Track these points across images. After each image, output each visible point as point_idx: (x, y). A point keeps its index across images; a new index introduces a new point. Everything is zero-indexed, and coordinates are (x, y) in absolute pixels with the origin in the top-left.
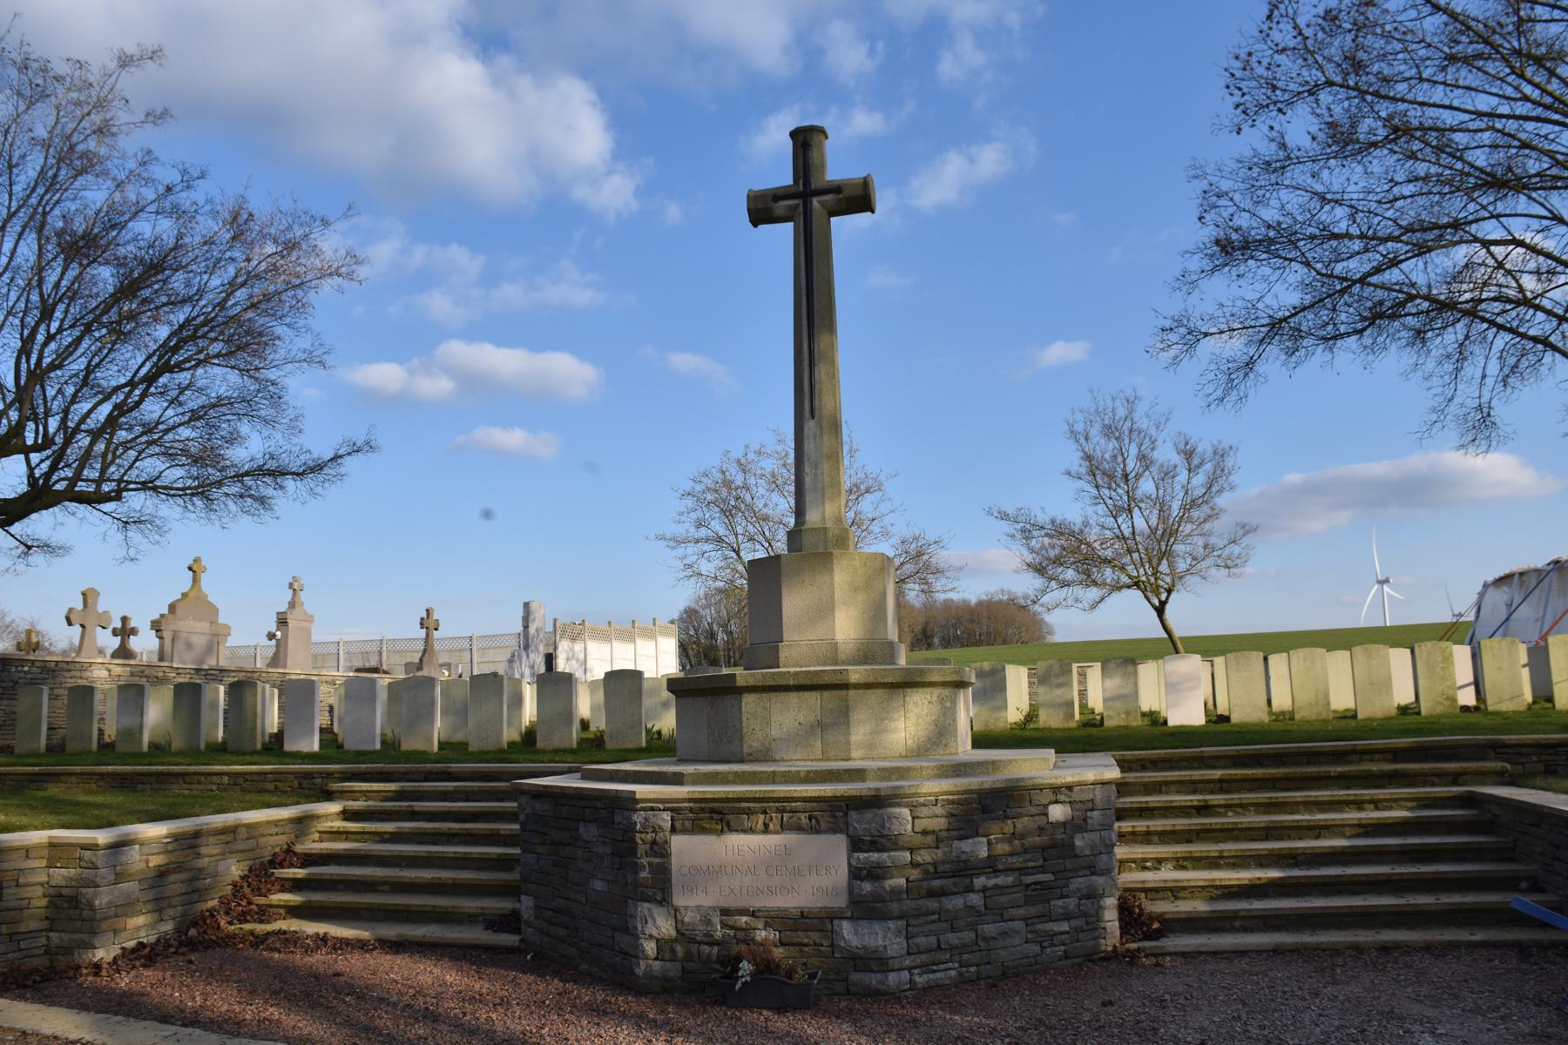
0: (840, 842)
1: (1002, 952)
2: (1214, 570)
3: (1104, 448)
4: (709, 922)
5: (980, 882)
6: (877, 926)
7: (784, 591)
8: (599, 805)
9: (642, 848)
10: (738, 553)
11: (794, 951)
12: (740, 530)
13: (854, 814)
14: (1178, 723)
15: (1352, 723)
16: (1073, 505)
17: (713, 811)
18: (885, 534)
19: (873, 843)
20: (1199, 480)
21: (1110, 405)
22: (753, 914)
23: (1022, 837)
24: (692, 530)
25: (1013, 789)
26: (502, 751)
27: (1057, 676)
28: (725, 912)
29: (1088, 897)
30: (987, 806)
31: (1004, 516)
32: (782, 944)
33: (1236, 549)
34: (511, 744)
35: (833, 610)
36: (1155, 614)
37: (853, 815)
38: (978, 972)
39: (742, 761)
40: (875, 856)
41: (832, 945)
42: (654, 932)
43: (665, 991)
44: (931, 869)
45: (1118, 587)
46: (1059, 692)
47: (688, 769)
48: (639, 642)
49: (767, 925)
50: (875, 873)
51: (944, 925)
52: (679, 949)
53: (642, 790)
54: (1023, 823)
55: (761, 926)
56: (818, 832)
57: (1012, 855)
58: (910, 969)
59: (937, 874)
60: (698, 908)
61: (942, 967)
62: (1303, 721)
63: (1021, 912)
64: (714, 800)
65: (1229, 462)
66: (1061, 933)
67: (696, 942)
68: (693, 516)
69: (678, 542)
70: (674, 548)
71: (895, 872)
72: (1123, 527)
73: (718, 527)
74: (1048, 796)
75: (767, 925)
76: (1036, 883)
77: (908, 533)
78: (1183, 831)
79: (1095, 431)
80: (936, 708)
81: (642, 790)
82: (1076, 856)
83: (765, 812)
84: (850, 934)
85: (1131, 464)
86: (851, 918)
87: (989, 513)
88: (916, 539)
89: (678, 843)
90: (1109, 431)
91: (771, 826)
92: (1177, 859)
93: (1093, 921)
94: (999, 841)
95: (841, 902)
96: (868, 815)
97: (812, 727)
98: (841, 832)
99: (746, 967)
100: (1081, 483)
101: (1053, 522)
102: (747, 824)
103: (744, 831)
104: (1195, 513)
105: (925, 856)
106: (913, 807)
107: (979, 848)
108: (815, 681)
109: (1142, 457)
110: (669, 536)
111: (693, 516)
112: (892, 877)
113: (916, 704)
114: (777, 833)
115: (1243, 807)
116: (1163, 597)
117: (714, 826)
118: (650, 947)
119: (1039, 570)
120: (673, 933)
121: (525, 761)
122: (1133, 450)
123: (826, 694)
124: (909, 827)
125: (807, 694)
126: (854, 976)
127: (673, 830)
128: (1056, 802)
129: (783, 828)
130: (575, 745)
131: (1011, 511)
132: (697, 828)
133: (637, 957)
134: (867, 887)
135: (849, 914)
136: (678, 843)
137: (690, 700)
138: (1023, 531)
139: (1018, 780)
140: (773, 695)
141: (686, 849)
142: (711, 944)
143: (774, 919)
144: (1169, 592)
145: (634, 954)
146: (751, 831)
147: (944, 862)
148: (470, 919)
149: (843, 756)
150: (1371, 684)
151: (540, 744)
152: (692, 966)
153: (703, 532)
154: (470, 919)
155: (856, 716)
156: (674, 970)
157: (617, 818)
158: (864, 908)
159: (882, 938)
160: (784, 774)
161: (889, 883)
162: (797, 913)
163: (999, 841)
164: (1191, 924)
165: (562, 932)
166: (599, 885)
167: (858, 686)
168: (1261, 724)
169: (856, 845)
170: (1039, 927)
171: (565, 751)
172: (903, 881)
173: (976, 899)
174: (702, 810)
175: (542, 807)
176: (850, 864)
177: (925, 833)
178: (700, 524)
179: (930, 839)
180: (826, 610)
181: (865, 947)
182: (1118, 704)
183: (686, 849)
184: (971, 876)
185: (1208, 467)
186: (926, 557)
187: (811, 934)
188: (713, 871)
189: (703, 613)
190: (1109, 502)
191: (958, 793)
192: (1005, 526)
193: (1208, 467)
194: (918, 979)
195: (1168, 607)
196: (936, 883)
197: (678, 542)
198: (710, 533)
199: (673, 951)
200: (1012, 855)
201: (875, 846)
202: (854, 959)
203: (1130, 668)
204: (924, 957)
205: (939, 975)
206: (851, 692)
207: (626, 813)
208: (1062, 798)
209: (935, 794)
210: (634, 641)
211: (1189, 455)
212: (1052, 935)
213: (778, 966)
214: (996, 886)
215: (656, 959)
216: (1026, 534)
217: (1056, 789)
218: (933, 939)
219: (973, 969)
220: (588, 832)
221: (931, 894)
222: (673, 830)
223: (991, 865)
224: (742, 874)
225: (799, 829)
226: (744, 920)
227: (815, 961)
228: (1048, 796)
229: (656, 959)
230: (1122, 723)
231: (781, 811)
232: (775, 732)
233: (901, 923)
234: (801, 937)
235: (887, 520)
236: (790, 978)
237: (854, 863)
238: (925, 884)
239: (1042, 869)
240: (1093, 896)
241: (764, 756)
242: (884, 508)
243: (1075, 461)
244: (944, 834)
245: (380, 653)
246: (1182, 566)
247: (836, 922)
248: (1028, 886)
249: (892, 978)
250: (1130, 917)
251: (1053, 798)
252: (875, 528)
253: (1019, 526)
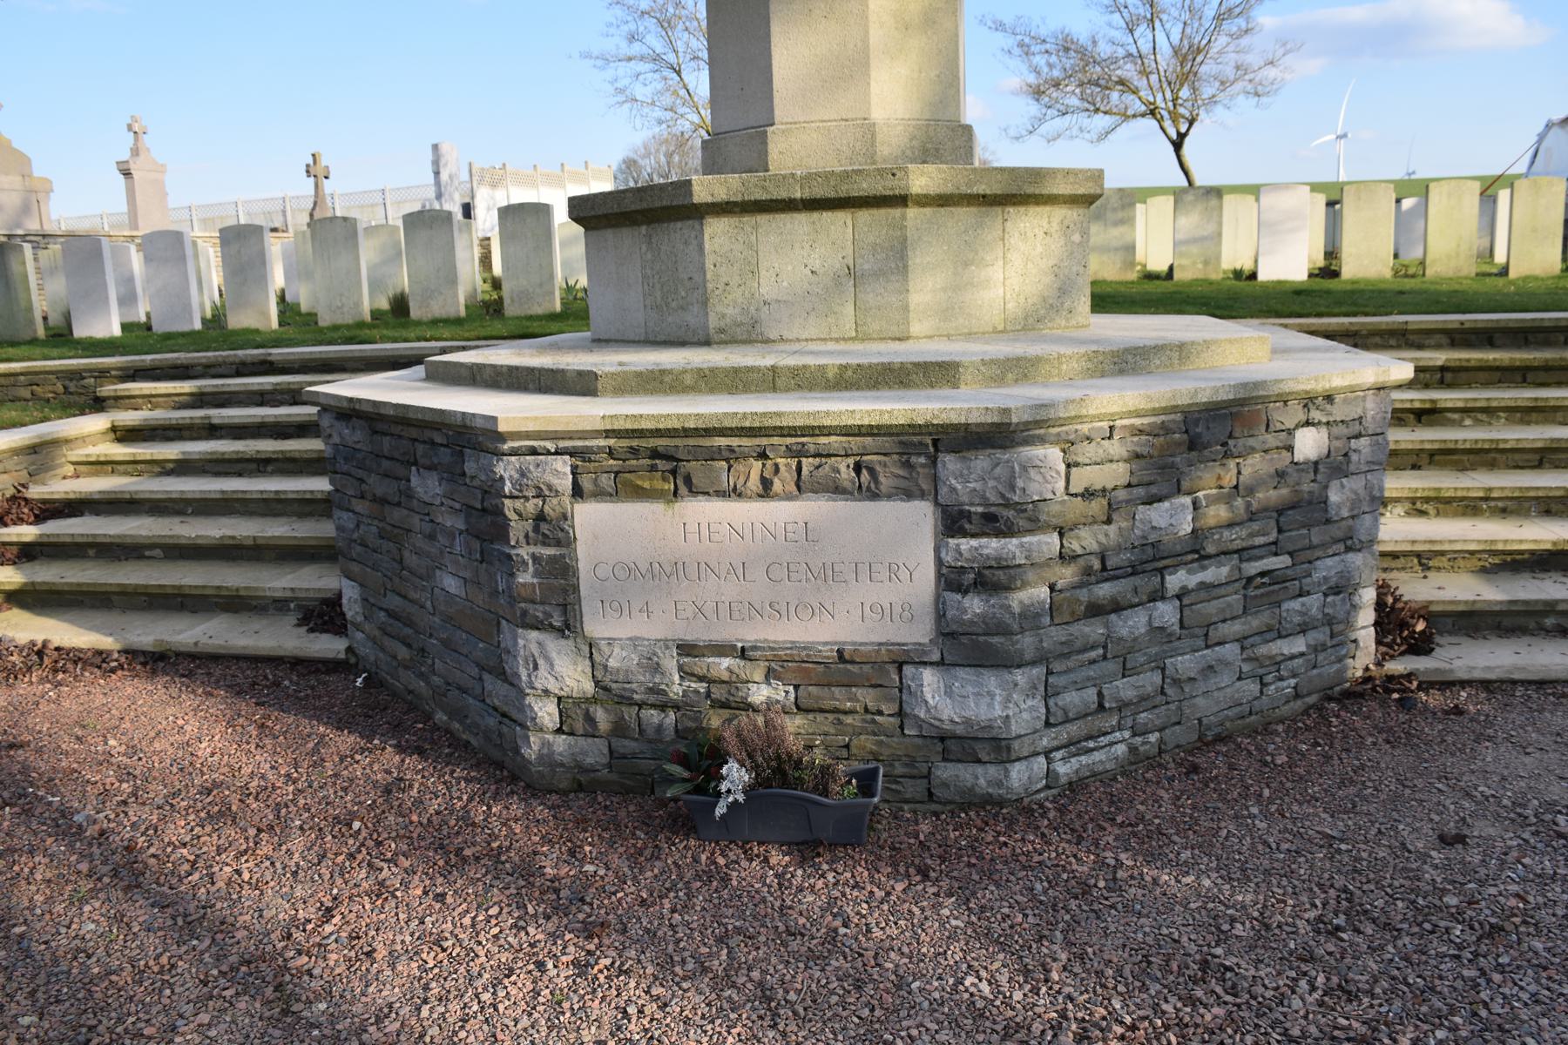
0: (920, 516)
1: (1200, 701)
2: (1241, 98)
4: (656, 668)
5: (1177, 580)
6: (991, 680)
7: (776, 29)
8: (439, 439)
9: (517, 529)
10: (679, 73)
11: (825, 722)
12: (680, 46)
13: (948, 464)
14: (1275, 277)
15: (1501, 281)
17: (655, 454)
19: (990, 518)
22: (743, 654)
23: (1251, 491)
24: (624, 44)
25: (1241, 402)
26: (361, 325)
27: (1114, 210)
28: (687, 649)
29: (1336, 590)
30: (1202, 433)
31: (1000, 26)
32: (799, 708)
33: (1271, 73)
34: (376, 314)
36: (1171, 148)
37: (950, 463)
38: (1161, 741)
39: (706, 343)
40: (992, 546)
41: (901, 713)
42: (553, 686)
43: (580, 787)
44: (1097, 565)
45: (1126, 117)
46: (1115, 232)
47: (604, 362)
49: (770, 675)
50: (990, 579)
51: (1112, 666)
52: (602, 716)
53: (510, 411)
54: (1254, 466)
55: (758, 676)
56: (874, 496)
57: (1230, 525)
58: (1047, 753)
59: (1106, 572)
60: (634, 641)
61: (1104, 740)
62: (1439, 280)
63: (1236, 628)
64: (657, 433)
66: (1293, 657)
67: (631, 703)
68: (625, 28)
69: (605, 60)
70: (602, 68)
71: (1031, 575)
73: (656, 43)
74: (1295, 414)
75: (770, 675)
76: (1262, 574)
78: (1409, 452)
80: (1057, 245)
81: (510, 411)
82: (1328, 521)
83: (763, 456)
84: (939, 696)
86: (940, 663)
89: (589, 518)
91: (777, 486)
92: (1413, 501)
93: (1337, 629)
94: (1212, 501)
95: (919, 633)
96: (981, 462)
97: (837, 281)
98: (922, 495)
99: (735, 776)
102: (724, 482)
103: (722, 494)
105: (1086, 540)
106: (1067, 445)
107: (1173, 518)
108: (844, 190)
110: (596, 53)
111: (625, 28)
112: (1025, 585)
113: (1023, 235)
114: (789, 497)
115: (1489, 412)
116: (1183, 130)
117: (660, 485)
118: (547, 712)
119: (1037, 93)
120: (589, 687)
121: (383, 339)
123: (864, 215)
124: (1061, 484)
125: (827, 216)
126: (946, 772)
127: (578, 492)
128: (1308, 423)
129: (801, 487)
130: (463, 313)
131: (1008, 20)
132: (625, 489)
133: (523, 726)
134: (975, 605)
135: (936, 657)
136: (589, 518)
137: (609, 234)
139: (1257, 385)
140: (763, 219)
141: (604, 529)
142: (662, 707)
143: (780, 664)
144: (1191, 123)
145: (515, 719)
146: (736, 493)
147: (1119, 549)
148: (274, 606)
149: (895, 331)
150: (1535, 230)
151: (415, 313)
152: (628, 746)
153: (637, 48)
154: (274, 606)
155: (917, 259)
156: (594, 753)
157: (470, 467)
158: (966, 647)
159: (999, 701)
160: (795, 372)
161: (1019, 599)
162: (830, 653)
163: (1212, 501)
164: (1474, 622)
165: (403, 653)
166: (451, 584)
167: (926, 201)
168: (1383, 281)
169: (953, 522)
170: (1263, 650)
171: (447, 322)
172: (1043, 592)
173: (1166, 613)
174: (634, 452)
175: (354, 435)
176: (939, 562)
177: (1088, 494)
178: (632, 38)
179: (1097, 507)
180: (851, 68)
181: (967, 722)
182: (1194, 249)
183: (604, 529)
184: (1161, 571)
187: (859, 692)
188: (659, 574)
189: (641, 162)
191: (1155, 412)
194: (1062, 769)
195: (1187, 140)
196: (1105, 591)
197: (605, 60)
198: (645, 51)
199: (590, 719)
200: (1230, 525)
201: (993, 524)
202: (942, 739)
203: (1214, 202)
204: (1074, 729)
205: (1097, 756)
206: (912, 212)
207: (485, 459)
208: (1316, 415)
209: (1112, 417)
212: (1277, 662)
213: (798, 764)
214: (1203, 586)
215: (559, 731)
217: (1309, 401)
218: (1091, 694)
219: (1153, 737)
220: (427, 486)
221: (1096, 610)
222: (578, 492)
223: (1196, 550)
224: (727, 585)
225: (837, 490)
226: (723, 665)
227: (866, 742)
228: (1295, 414)
229: (559, 731)
230: (1201, 276)
231: (798, 453)
232: (767, 289)
233: (1038, 671)
234: (838, 697)
236: (825, 793)
237: (948, 558)
238: (1083, 595)
239: (1275, 549)
240: (1343, 588)
241: (749, 334)
244: (1122, 495)
245: (284, 212)
246: (1207, 91)
247: (908, 670)
248: (1250, 579)
249: (1018, 776)
250: (1394, 623)
251: (1302, 417)
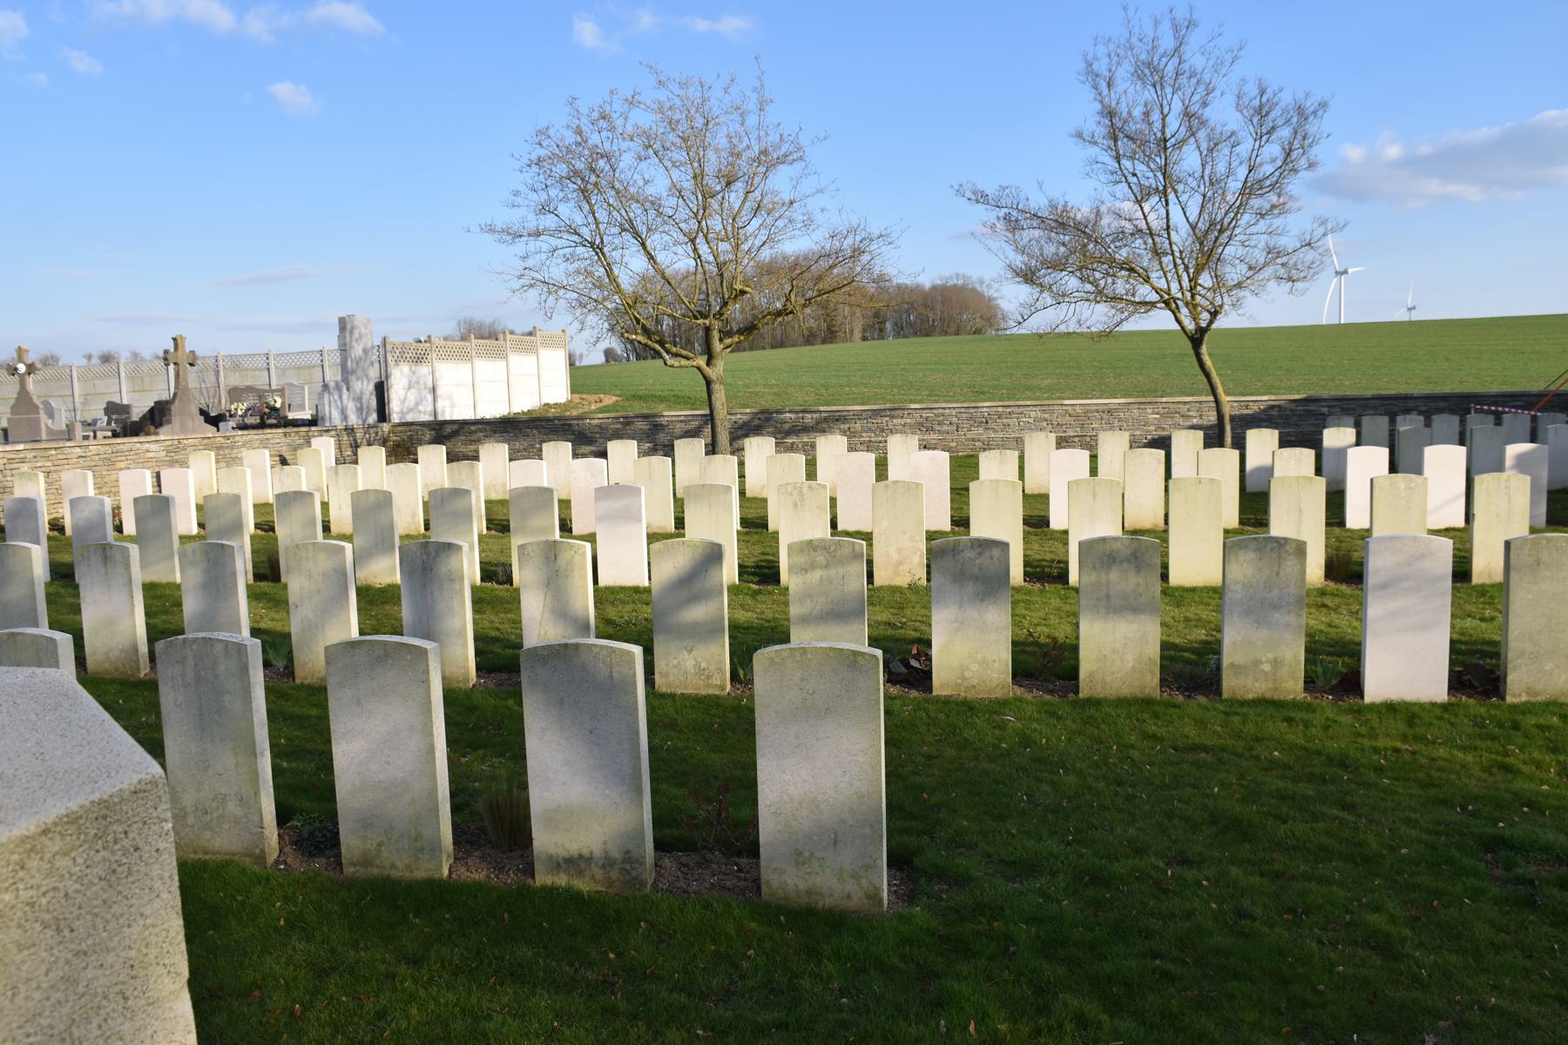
2: (1272, 283)
3: (1132, 97)
16: (1085, 186)
18: (808, 224)
20: (1273, 150)
21: (1151, 33)
24: (531, 216)
31: (981, 198)
35: (354, 514)
36: (1189, 345)
48: (543, 352)
65: (1312, 127)
72: (1151, 217)
77: (841, 224)
79: (1123, 73)
85: (1173, 123)
87: (960, 192)
88: (853, 231)
90: (1150, 72)
100: (1095, 151)
101: (1053, 207)
104: (1255, 202)
109: (1188, 115)
119: (1028, 276)
122: (1177, 106)
131: (991, 190)
138: (1007, 218)
153: (549, 221)
185: (1285, 133)
186: (865, 258)
190: (1133, 180)
192: (992, 215)
193: (1285, 133)
210: (506, 358)
211: (1261, 112)
216: (1012, 225)
235: (813, 204)
242: (807, 186)
243: (1088, 116)
246: (1232, 274)
252: (797, 213)
253: (1002, 212)
